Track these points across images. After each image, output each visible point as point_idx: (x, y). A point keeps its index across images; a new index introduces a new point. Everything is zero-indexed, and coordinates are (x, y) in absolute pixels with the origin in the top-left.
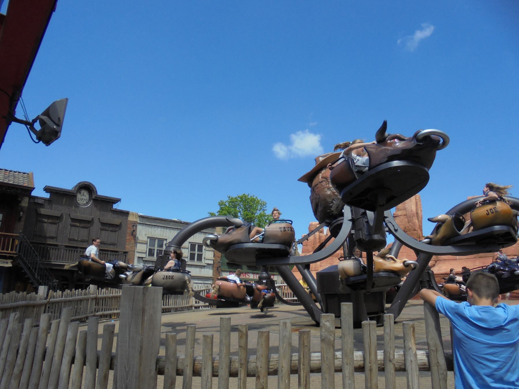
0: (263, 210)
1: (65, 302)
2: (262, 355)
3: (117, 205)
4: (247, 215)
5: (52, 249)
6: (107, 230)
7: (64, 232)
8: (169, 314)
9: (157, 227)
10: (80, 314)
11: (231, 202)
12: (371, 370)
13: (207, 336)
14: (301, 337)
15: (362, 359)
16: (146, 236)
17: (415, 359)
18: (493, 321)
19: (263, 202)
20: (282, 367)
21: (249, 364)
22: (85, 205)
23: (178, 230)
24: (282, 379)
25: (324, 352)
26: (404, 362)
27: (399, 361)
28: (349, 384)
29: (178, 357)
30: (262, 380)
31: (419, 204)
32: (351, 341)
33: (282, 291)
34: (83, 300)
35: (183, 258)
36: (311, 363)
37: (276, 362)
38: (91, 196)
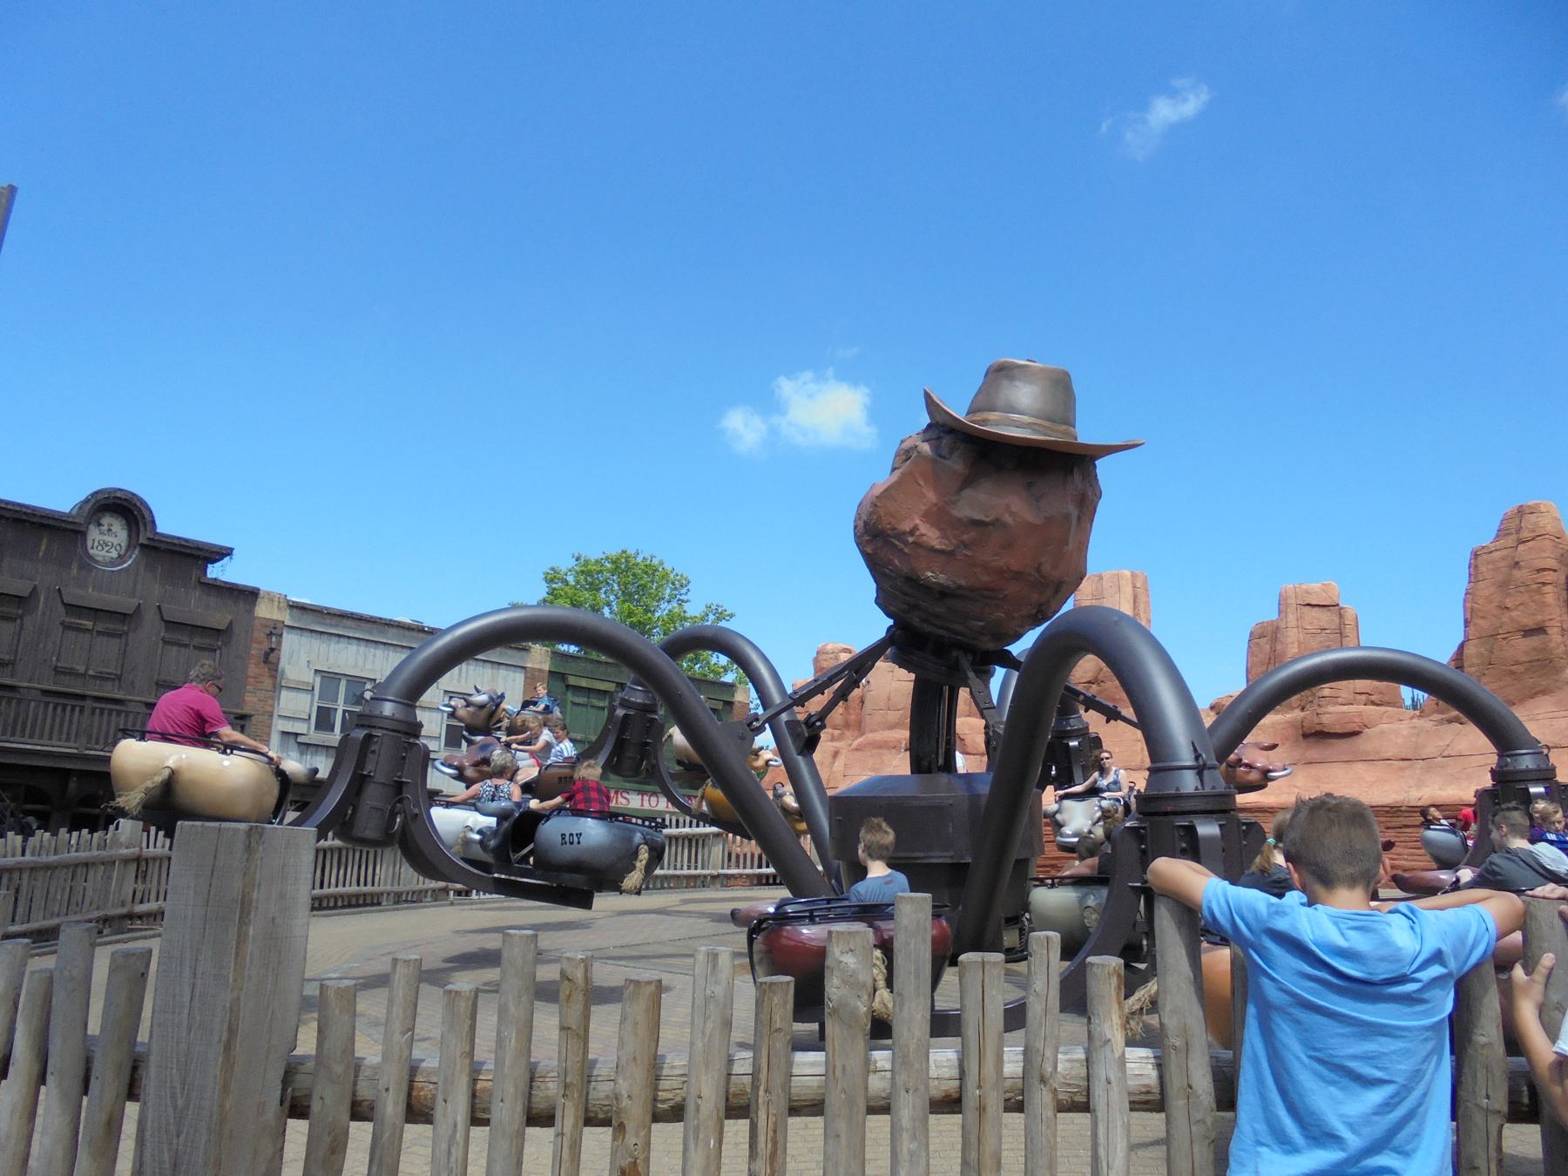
0: (679, 600)
1: (32, 869)
2: (635, 1058)
3: (221, 569)
4: (630, 614)
5: (114, 713)
6: (186, 646)
7: (41, 646)
8: (372, 912)
9: (346, 640)
10: (81, 909)
11: (582, 572)
12: (982, 1109)
13: (456, 992)
14: (763, 1001)
15: (955, 1073)
16: (311, 669)
17: (1120, 1075)
18: (1382, 959)
19: (679, 577)
20: (700, 1097)
21: (592, 1083)
22: (113, 563)
23: (404, 650)
24: (697, 1138)
25: (834, 1051)
26: (1086, 1083)
27: (1072, 1082)
28: (911, 1154)
29: (359, 1058)
30: (631, 1139)
31: (1142, 599)
32: (922, 1015)
33: (726, 846)
34: (94, 864)
35: (423, 741)
36: (792, 1085)
37: (678, 1078)
38: (134, 535)
